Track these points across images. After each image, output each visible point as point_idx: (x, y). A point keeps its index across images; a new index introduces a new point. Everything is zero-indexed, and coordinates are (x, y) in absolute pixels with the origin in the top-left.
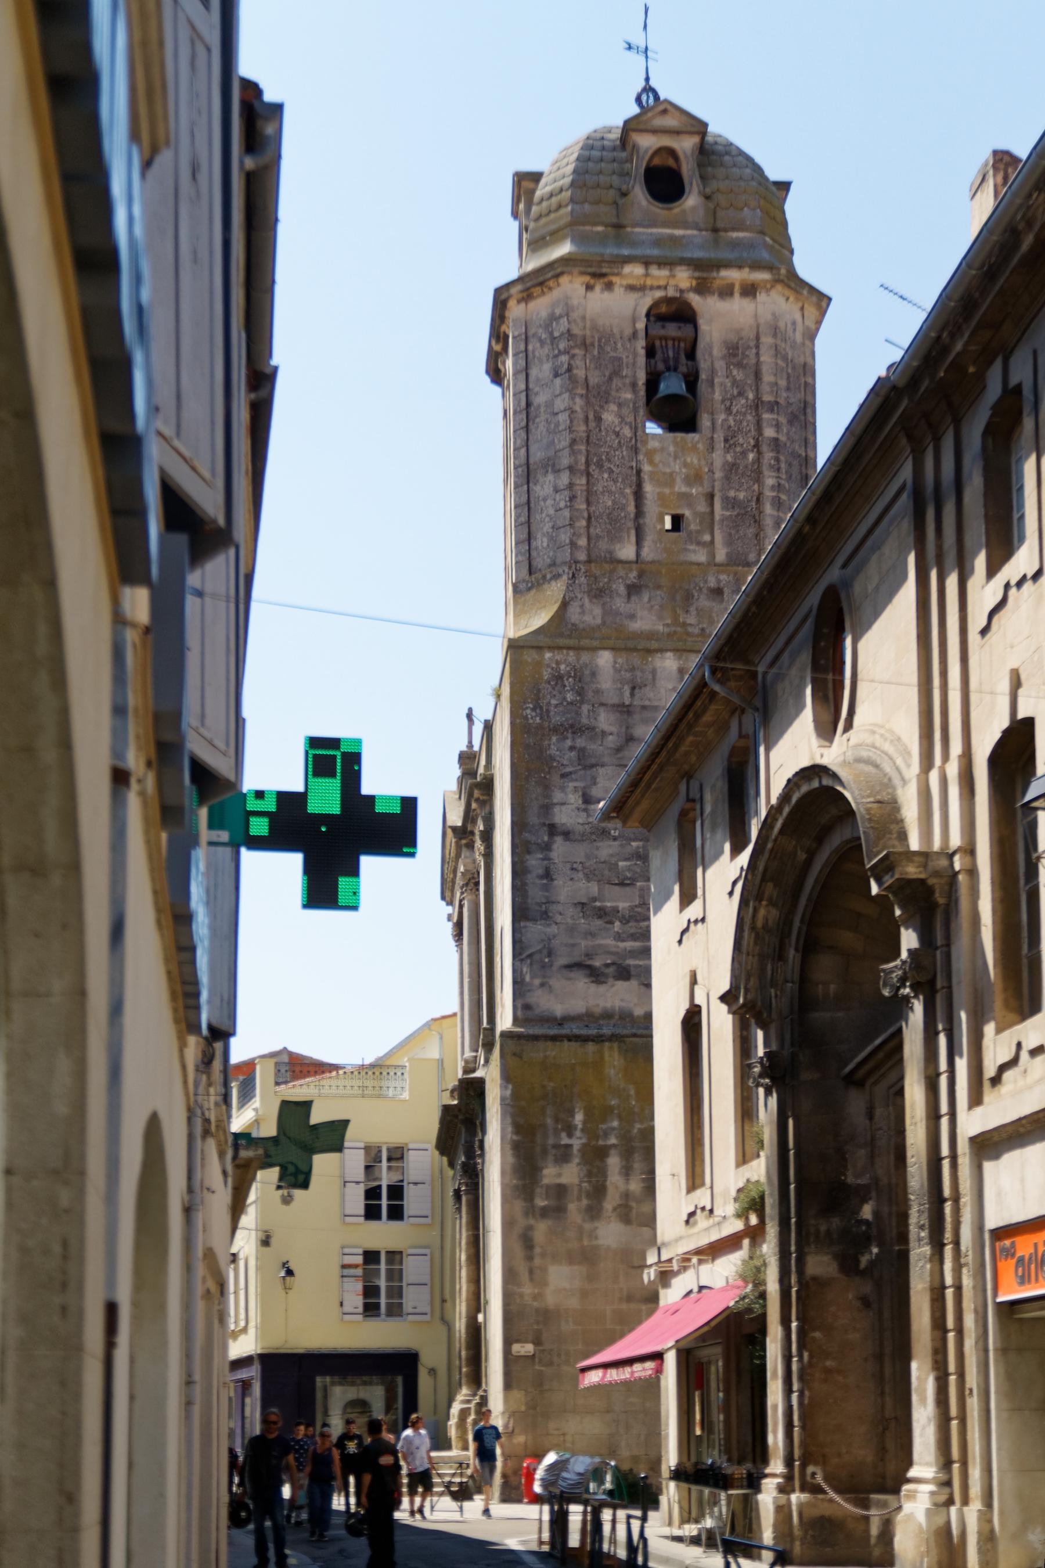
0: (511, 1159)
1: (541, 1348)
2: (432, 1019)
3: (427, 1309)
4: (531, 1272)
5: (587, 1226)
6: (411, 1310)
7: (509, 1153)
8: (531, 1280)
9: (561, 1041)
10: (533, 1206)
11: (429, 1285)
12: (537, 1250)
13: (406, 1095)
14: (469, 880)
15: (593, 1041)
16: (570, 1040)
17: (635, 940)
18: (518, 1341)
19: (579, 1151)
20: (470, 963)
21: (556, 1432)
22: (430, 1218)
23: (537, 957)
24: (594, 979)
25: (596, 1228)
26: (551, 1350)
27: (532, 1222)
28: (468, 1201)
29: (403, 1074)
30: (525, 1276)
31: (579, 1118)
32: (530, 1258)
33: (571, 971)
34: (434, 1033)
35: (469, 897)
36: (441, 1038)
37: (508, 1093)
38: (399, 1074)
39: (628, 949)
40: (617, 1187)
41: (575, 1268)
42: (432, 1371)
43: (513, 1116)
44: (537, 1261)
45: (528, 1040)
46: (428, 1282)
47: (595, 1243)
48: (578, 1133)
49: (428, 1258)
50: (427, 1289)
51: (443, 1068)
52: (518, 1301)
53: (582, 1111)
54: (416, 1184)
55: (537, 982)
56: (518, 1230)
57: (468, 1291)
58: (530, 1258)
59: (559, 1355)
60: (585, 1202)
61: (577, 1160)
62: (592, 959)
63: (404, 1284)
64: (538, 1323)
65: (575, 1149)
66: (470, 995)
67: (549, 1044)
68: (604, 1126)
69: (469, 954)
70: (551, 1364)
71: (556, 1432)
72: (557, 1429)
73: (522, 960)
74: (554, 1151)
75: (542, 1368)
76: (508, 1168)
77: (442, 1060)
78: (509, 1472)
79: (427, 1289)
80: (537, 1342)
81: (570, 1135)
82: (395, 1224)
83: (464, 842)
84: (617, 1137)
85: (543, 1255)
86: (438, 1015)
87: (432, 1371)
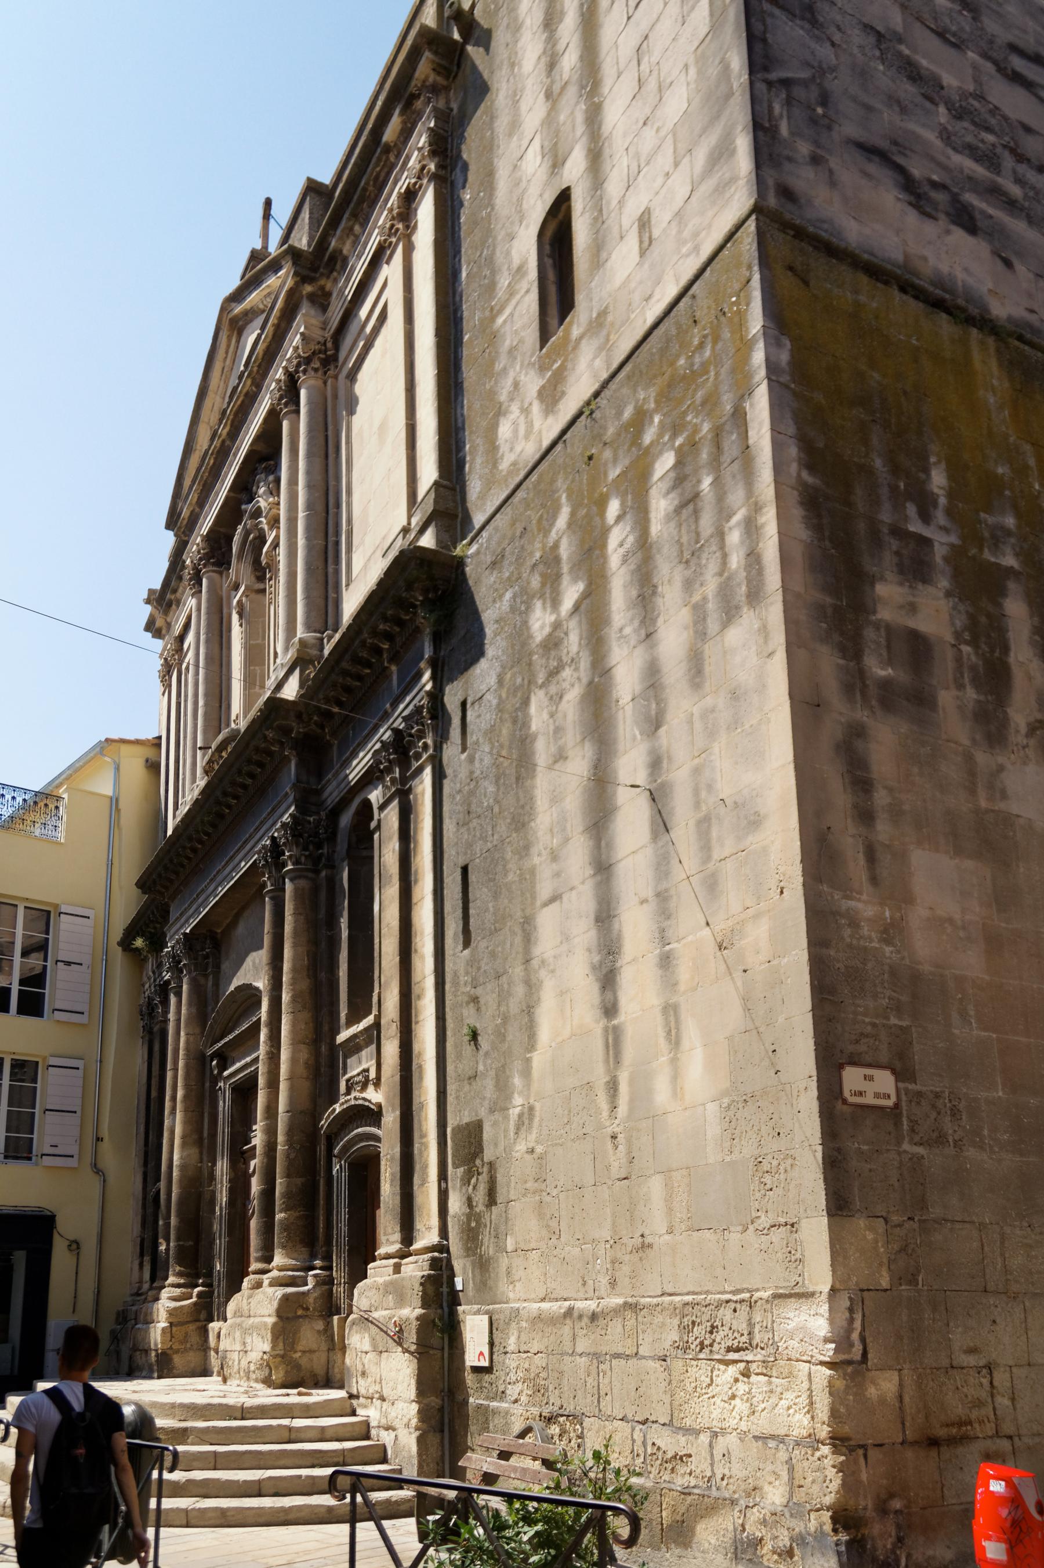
0: (801, 532)
1: (911, 1086)
2: (107, 740)
3: (74, 1150)
4: (871, 855)
5: (982, 758)
6: (48, 1150)
7: (797, 512)
8: (874, 880)
9: (886, 283)
10: (861, 673)
11: (79, 1113)
12: (881, 798)
13: (61, 836)
14: (314, 353)
15: (949, 312)
16: (903, 290)
17: (977, 160)
18: (855, 1061)
19: (946, 559)
20: (310, 486)
21: (971, 1360)
22: (86, 1014)
23: (798, 92)
24: (912, 199)
25: (1001, 769)
26: (937, 1096)
27: (862, 715)
28: (298, 894)
29: (57, 808)
30: (856, 867)
31: (938, 480)
32: (865, 816)
33: (870, 160)
34: (107, 759)
35: (312, 382)
36: (117, 769)
37: (784, 357)
38: (52, 806)
39: (966, 171)
40: (1030, 678)
41: (969, 864)
42: (75, 1246)
43: (799, 419)
44: (883, 829)
45: (815, 248)
46: (78, 1109)
47: (1001, 806)
48: (940, 517)
49: (80, 1073)
50: (75, 1119)
51: (118, 810)
52: (847, 932)
53: (943, 465)
54: (68, 963)
55: (804, 148)
56: (831, 730)
57: (293, 1061)
58: (865, 816)
59: (955, 1113)
60: (971, 694)
61: (944, 583)
62: (905, 155)
63: (37, 1111)
64: (898, 1009)
65: (940, 552)
66: (308, 539)
67: (864, 279)
68: (991, 520)
69: (308, 472)
70: (940, 1139)
71: (971, 1360)
72: (972, 1351)
73: (770, 84)
74: (895, 544)
75: (920, 1150)
76: (797, 552)
77: (117, 800)
78: (866, 1504)
79: (75, 1119)
80: (903, 1073)
81: (926, 517)
82: (29, 1022)
83: (308, 289)
84: (1017, 555)
85: (896, 813)
86: (115, 737)
87: (75, 1246)
